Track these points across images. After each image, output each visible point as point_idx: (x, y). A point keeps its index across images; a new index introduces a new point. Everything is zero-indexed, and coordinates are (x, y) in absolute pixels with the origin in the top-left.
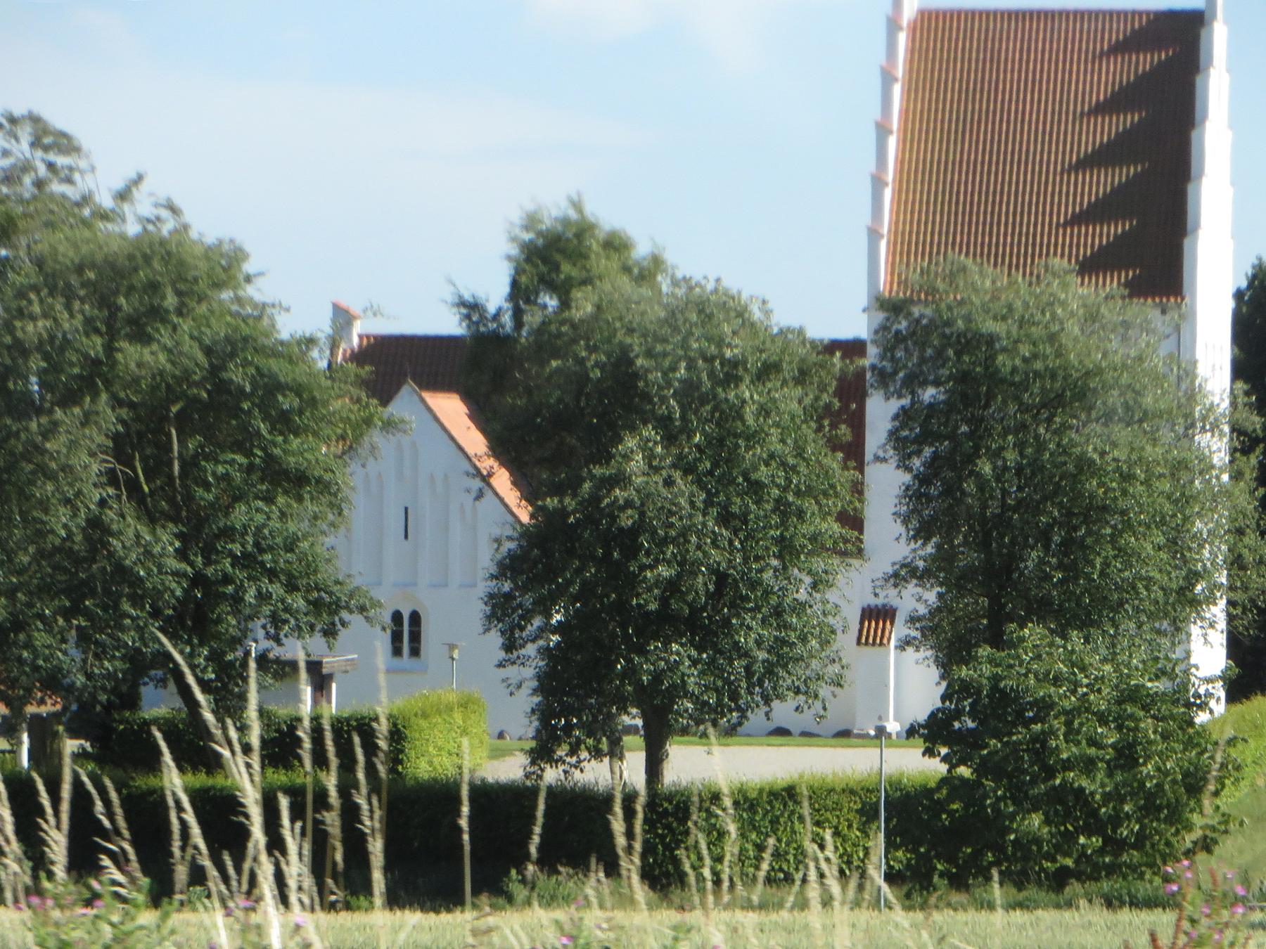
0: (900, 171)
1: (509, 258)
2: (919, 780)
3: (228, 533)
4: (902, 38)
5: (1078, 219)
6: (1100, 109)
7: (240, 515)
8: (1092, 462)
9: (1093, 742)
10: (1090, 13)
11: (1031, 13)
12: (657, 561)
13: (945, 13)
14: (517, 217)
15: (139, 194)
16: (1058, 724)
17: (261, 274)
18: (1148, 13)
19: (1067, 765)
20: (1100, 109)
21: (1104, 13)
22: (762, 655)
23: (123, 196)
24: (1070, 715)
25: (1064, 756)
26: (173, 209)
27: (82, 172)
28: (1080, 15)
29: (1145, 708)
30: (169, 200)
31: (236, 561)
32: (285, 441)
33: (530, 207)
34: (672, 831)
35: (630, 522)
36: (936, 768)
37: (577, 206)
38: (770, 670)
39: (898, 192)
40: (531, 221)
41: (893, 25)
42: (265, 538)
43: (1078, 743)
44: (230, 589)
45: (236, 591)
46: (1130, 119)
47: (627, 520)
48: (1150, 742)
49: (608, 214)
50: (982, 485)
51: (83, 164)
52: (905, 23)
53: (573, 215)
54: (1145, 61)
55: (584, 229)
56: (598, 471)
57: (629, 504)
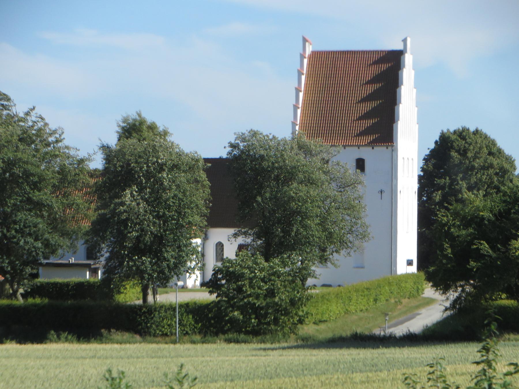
0: (303, 104)
1: (118, 132)
2: (206, 303)
3: (15, 222)
4: (306, 61)
5: (360, 118)
6: (369, 83)
7: (20, 216)
8: (293, 197)
9: (259, 288)
10: (367, 51)
11: (348, 52)
12: (133, 230)
13: (327, 52)
14: (120, 118)
15: (33, 113)
16: (247, 282)
17: (100, 140)
18: (385, 51)
19: (250, 296)
20: (369, 83)
21: (371, 51)
22: (172, 261)
23: (27, 114)
24: (251, 279)
25: (249, 293)
26: (42, 118)
27: (11, 106)
28: (363, 52)
29: (279, 277)
30: (40, 115)
31: (17, 231)
32: (34, 192)
33: (125, 115)
34: (147, 318)
35: (125, 217)
36: (213, 297)
37: (139, 115)
38: (176, 266)
39: (303, 111)
40: (125, 121)
41: (302, 57)
42: (27, 223)
43: (254, 289)
44: (15, 240)
45: (17, 241)
46: (379, 85)
47: (124, 217)
48: (279, 289)
49: (149, 118)
50: (259, 204)
51: (12, 104)
52: (307, 56)
53: (137, 117)
54: (384, 67)
55: (142, 122)
56: (117, 200)
57: (125, 211)
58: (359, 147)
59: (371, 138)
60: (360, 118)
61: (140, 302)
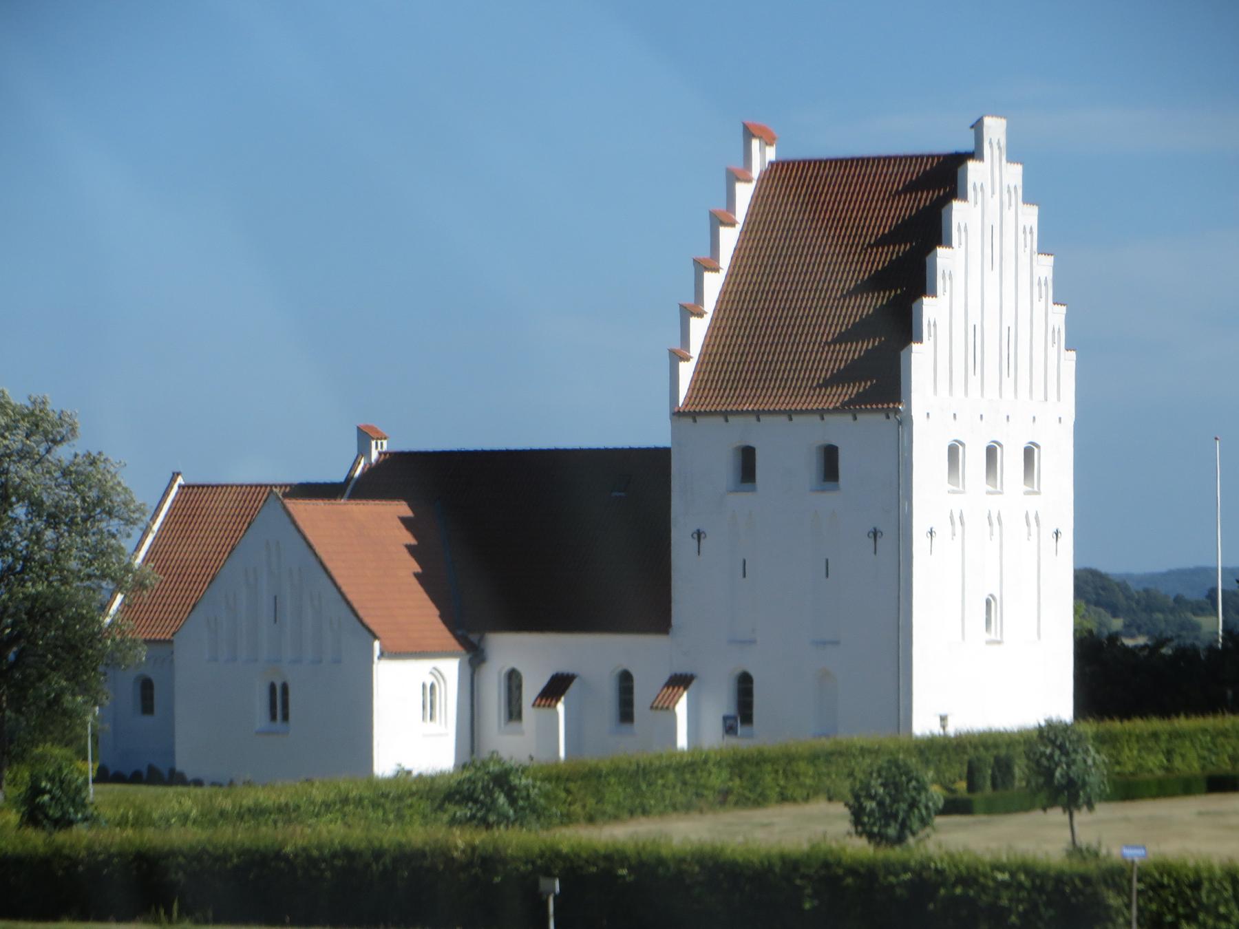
5: (842, 338)
18: (939, 156)
20: (883, 241)
46: (903, 248)
58: (822, 413)
59: (852, 390)
60: (842, 338)
61: (941, 731)
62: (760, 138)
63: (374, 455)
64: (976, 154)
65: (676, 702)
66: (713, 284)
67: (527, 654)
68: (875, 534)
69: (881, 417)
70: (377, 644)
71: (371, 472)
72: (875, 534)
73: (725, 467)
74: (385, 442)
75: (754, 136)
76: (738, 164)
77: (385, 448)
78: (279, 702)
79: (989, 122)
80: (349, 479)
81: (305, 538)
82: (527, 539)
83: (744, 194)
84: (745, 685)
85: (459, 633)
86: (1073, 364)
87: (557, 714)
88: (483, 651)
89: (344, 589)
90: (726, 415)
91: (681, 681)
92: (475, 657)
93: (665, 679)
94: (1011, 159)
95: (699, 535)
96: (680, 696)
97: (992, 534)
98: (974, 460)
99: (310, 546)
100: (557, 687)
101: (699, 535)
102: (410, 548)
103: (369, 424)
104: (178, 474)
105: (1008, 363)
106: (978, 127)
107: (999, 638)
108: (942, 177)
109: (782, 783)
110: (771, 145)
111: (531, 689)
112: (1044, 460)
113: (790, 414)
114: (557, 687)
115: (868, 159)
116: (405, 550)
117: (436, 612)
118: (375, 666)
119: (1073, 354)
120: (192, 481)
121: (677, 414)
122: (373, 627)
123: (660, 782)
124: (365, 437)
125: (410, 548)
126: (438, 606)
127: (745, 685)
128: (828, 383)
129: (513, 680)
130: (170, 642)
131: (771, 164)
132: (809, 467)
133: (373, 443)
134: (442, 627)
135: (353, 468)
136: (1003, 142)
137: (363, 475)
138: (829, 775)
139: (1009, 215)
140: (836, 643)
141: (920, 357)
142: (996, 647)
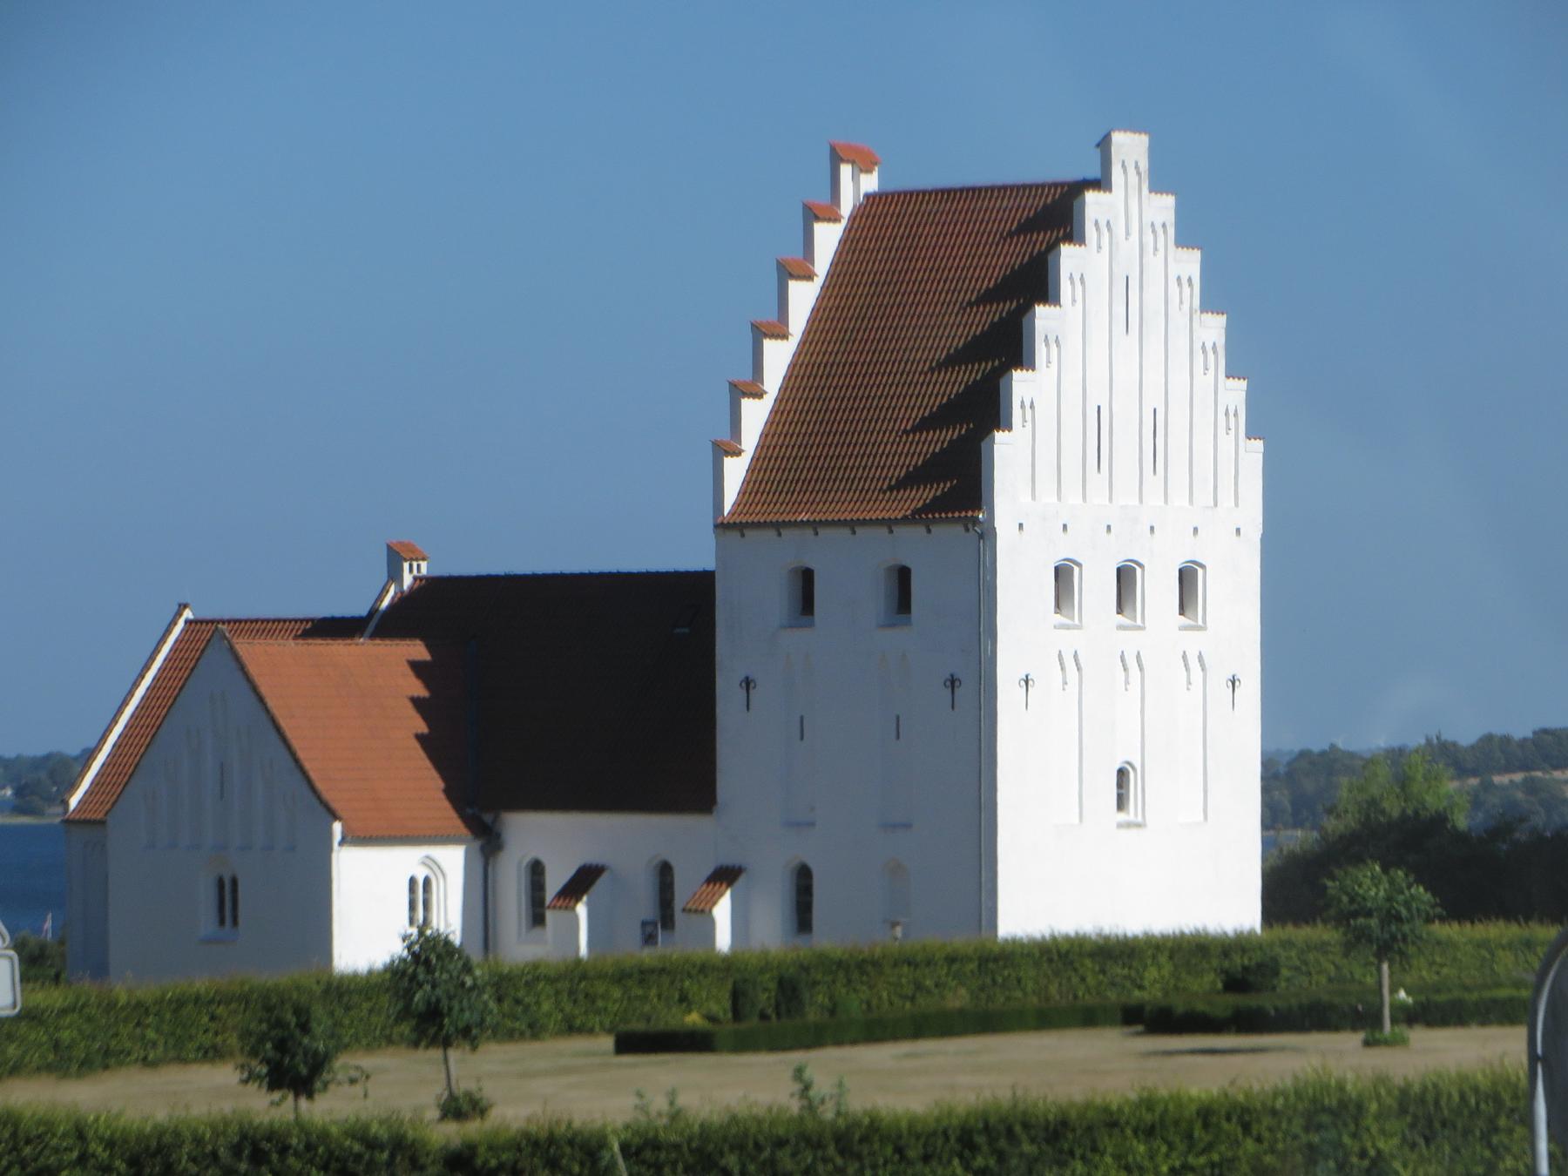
5: (925, 425)
58: (889, 524)
59: (928, 494)
60: (925, 425)
62: (853, 163)
63: (408, 580)
64: (1101, 183)
65: (715, 903)
66: (778, 357)
67: (548, 838)
68: (953, 682)
69: (958, 529)
70: (337, 827)
71: (405, 603)
72: (953, 682)
73: (777, 596)
74: (424, 565)
75: (842, 160)
76: (821, 198)
77: (424, 571)
78: (227, 897)
79: (1118, 138)
80: (373, 612)
81: (255, 689)
82: (560, 690)
83: (828, 238)
84: (803, 880)
85: (469, 811)
86: (1260, 456)
87: (576, 919)
88: (498, 836)
89: (301, 755)
90: (778, 526)
91: (725, 876)
92: (486, 840)
93: (708, 870)
94: (1156, 188)
95: (748, 683)
96: (722, 895)
97: (1127, 682)
98: (1096, 586)
99: (261, 699)
100: (582, 882)
101: (748, 683)
102: (417, 702)
103: (405, 539)
104: (186, 606)
105: (1155, 456)
106: (1104, 144)
107: (1140, 819)
108: (1055, 214)
109: (568, 1008)
110: (869, 171)
111: (554, 882)
112: (1211, 587)
113: (852, 525)
114: (582, 882)
115: (980, 189)
116: (410, 705)
117: (441, 785)
118: (334, 856)
119: (1258, 445)
120: (209, 615)
121: (722, 527)
122: (334, 805)
123: (366, 1006)
124: (395, 559)
125: (417, 702)
126: (444, 778)
127: (803, 880)
128: (902, 484)
129: (536, 871)
130: (102, 823)
131: (867, 196)
132: (875, 599)
133: (406, 565)
134: (446, 804)
135: (380, 598)
136: (1144, 165)
137: (392, 606)
138: (645, 998)
139: (1155, 263)
140: (908, 826)
141: (1009, 454)
142: (1133, 832)
